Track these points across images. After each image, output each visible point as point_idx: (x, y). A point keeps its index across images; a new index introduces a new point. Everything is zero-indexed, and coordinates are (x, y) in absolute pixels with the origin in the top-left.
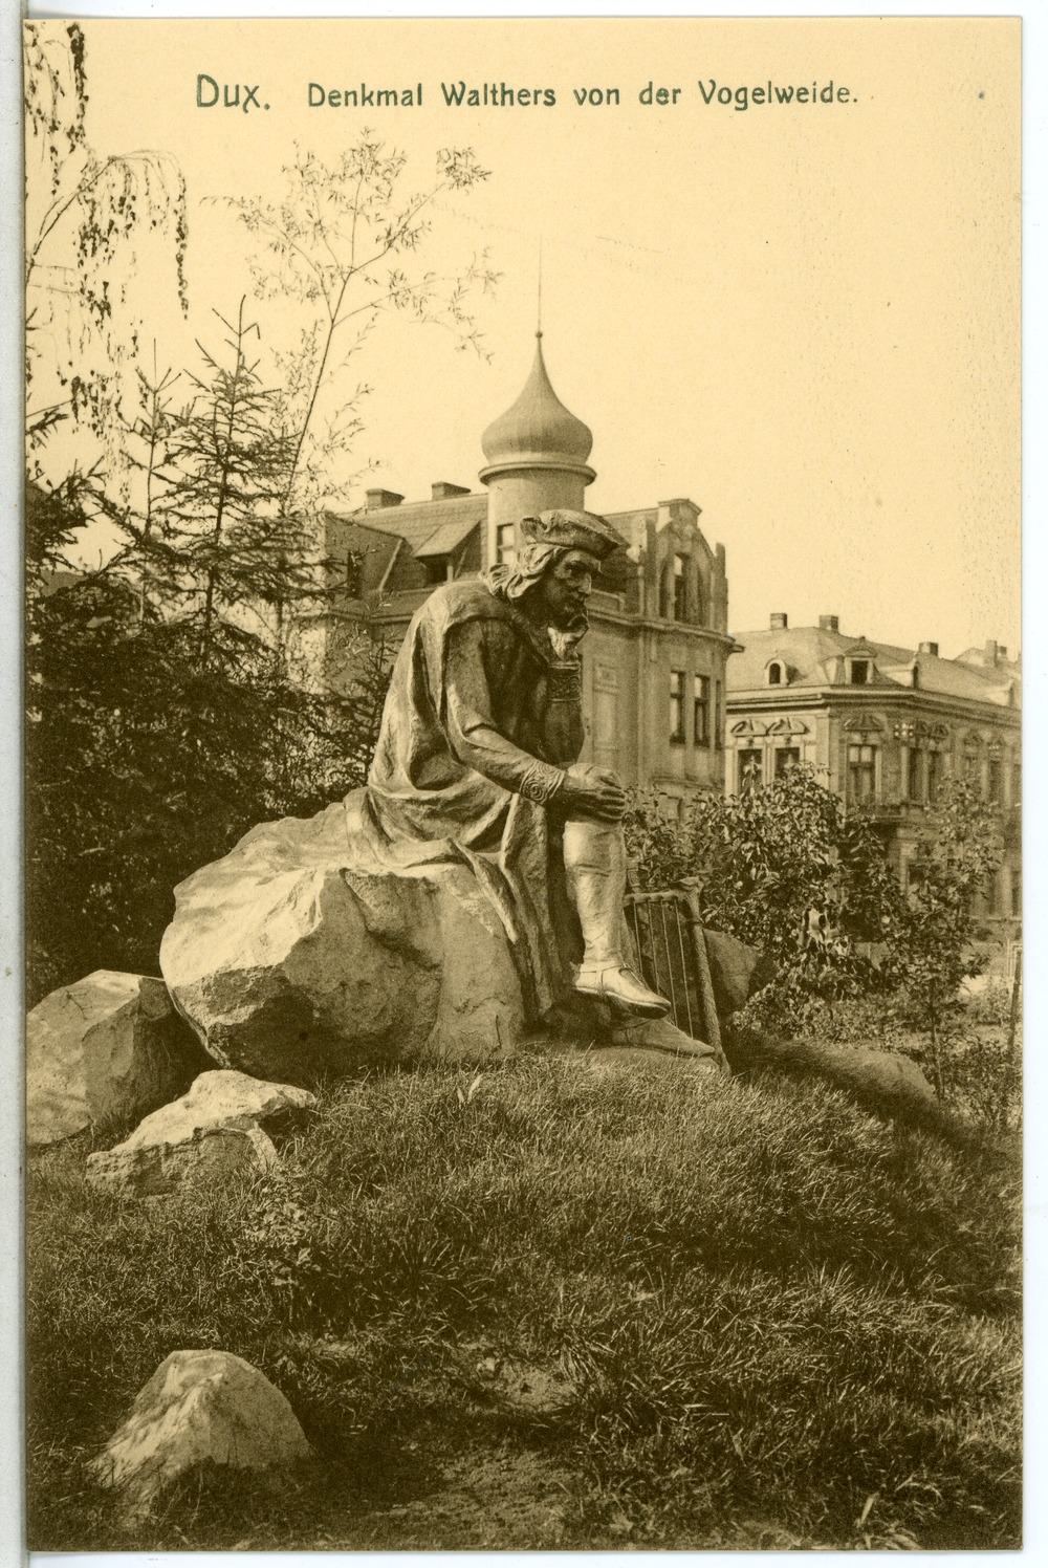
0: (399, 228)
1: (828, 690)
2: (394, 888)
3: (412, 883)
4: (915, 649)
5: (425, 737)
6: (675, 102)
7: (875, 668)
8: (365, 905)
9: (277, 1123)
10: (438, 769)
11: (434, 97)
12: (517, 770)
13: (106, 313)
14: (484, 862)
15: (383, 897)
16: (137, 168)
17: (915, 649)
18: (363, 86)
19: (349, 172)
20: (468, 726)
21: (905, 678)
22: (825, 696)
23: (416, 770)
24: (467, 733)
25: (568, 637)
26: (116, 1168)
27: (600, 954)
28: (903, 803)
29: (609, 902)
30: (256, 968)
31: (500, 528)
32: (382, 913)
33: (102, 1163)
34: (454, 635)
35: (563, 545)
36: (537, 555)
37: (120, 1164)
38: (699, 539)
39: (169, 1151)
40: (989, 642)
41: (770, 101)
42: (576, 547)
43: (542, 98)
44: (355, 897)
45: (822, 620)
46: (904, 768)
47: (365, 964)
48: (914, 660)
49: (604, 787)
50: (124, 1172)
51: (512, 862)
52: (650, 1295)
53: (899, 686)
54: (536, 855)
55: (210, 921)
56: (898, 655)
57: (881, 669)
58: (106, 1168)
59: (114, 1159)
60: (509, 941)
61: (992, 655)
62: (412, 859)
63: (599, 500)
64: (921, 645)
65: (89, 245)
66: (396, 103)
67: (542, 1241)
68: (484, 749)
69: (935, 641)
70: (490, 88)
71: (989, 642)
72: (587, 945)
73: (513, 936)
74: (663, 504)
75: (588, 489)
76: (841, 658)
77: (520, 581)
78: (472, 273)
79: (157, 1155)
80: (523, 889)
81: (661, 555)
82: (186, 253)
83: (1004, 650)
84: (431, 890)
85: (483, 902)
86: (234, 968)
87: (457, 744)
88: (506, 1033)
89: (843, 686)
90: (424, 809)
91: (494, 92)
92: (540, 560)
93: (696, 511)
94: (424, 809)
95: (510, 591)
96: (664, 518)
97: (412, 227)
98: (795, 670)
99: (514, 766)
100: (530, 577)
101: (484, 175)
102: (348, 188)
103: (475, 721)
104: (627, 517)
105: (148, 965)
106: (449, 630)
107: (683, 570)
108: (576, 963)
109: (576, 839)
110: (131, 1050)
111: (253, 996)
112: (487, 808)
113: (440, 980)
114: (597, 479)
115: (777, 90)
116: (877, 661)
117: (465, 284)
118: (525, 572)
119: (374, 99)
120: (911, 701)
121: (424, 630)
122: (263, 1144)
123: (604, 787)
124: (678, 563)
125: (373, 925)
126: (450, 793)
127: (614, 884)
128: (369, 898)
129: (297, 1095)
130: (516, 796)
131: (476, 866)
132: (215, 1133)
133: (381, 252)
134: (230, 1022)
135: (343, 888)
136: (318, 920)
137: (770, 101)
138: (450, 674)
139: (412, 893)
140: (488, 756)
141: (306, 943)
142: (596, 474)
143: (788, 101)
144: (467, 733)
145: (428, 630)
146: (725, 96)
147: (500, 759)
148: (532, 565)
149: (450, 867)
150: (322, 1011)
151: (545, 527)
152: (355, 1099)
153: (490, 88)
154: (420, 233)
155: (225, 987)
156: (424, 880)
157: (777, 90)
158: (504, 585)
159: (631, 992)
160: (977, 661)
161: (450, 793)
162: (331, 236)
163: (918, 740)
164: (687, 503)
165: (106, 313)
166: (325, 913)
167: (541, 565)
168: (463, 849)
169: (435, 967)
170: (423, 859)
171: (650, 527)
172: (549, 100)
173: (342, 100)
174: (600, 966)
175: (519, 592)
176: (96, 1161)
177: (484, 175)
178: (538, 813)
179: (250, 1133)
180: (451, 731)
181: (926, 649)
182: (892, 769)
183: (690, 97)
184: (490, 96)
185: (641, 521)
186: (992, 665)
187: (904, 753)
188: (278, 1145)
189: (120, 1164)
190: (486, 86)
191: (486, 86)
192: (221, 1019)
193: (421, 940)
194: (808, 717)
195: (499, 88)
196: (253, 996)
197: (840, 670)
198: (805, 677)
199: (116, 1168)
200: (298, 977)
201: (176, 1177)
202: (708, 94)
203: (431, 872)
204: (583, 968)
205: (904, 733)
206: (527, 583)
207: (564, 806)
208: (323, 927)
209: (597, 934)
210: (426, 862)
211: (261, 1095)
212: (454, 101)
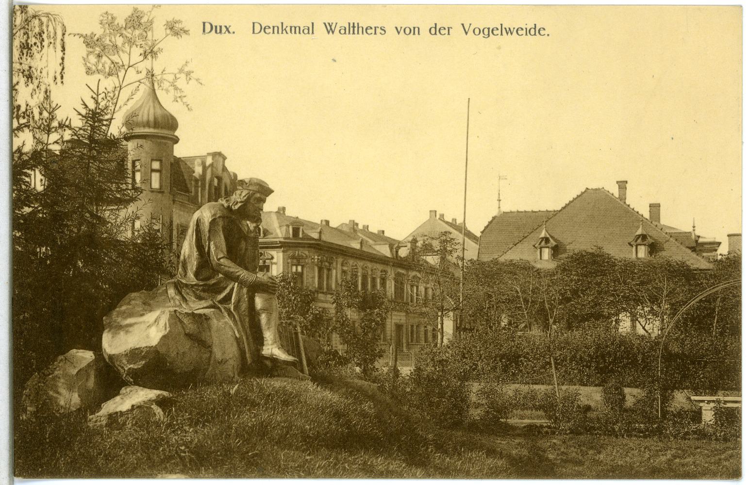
0: (150, 51)
1: (282, 240)
2: (194, 318)
3: (200, 315)
4: (319, 222)
5: (200, 261)
6: (449, 34)
7: (303, 231)
8: (184, 324)
9: (162, 402)
10: (206, 273)
11: (320, 29)
12: (238, 274)
13: (30, 79)
14: (225, 308)
15: (190, 321)
16: (44, 20)
17: (319, 222)
18: (282, 23)
19: (129, 26)
20: (219, 257)
21: (315, 236)
22: (280, 242)
23: (197, 275)
24: (219, 260)
25: (254, 225)
26: (100, 421)
27: (270, 342)
28: (316, 291)
29: (273, 323)
30: (146, 347)
31: (134, 162)
32: (191, 327)
33: (94, 420)
34: (213, 223)
35: (254, 191)
36: (243, 194)
37: (102, 420)
38: (224, 169)
39: (122, 413)
40: (350, 221)
41: (502, 34)
42: (258, 192)
43: (378, 30)
44: (180, 321)
45: (279, 209)
46: (316, 274)
47: (186, 345)
48: (320, 228)
49: (271, 281)
50: (104, 423)
51: (237, 307)
52: (311, 457)
53: (313, 239)
54: (244, 306)
55: (131, 329)
56: (312, 225)
57: (305, 231)
58: (96, 421)
59: (99, 418)
60: (236, 337)
61: (352, 227)
62: (198, 307)
63: (179, 151)
64: (322, 221)
65: (25, 51)
66: (300, 33)
67: (271, 440)
68: (225, 266)
69: (327, 219)
70: (351, 25)
71: (350, 221)
72: (265, 339)
73: (238, 335)
74: (209, 154)
75: (176, 146)
76: (288, 226)
77: (237, 204)
78: (181, 71)
79: (117, 415)
80: (240, 318)
81: (208, 177)
82: (65, 57)
83: (357, 224)
84: (207, 318)
85: (226, 323)
86: (138, 347)
87: (214, 263)
88: (236, 373)
89: (289, 238)
90: (200, 288)
91: (354, 27)
92: (245, 196)
93: (224, 158)
94: (200, 288)
95: (233, 207)
96: (209, 161)
97: (155, 49)
98: (267, 231)
99: (237, 272)
100: (241, 202)
101: (186, 32)
102: (128, 33)
103: (222, 255)
104: (193, 158)
105: (97, 347)
106: (212, 221)
107: (218, 184)
108: (260, 346)
109: (259, 302)
110: (93, 379)
111: (144, 358)
112: (225, 288)
113: (211, 352)
114: (180, 141)
115: (505, 28)
116: (304, 228)
117: (178, 76)
118: (239, 200)
119: (288, 29)
120: (318, 246)
121: (200, 220)
122: (158, 410)
123: (271, 281)
124: (216, 180)
125: (187, 331)
126: (213, 281)
127: (275, 315)
128: (185, 321)
129: (165, 393)
130: (236, 284)
131: (223, 310)
132: (139, 407)
133: (142, 59)
134: (136, 367)
135: (175, 318)
136: (168, 330)
137: (502, 34)
138: (212, 238)
139: (200, 319)
140: (227, 269)
141: (164, 337)
142: (179, 139)
143: (333, 32)
144: (219, 260)
145: (201, 220)
146: (477, 31)
147: (231, 270)
148: (242, 197)
149: (213, 310)
150: (170, 363)
151: (247, 184)
152: (190, 395)
153: (351, 25)
154: (158, 53)
155: (134, 354)
156: (204, 314)
157: (505, 28)
158: (231, 205)
159: (282, 355)
160: (345, 229)
161: (213, 281)
162: (121, 53)
163: (322, 263)
164: (220, 154)
165: (30, 79)
166: (170, 326)
167: (245, 198)
168: (216, 303)
169: (210, 347)
170: (202, 307)
171: (203, 164)
172: (383, 32)
173: (271, 30)
174: (270, 347)
175: (237, 207)
176: (92, 419)
177: (186, 32)
178: (245, 290)
179: (152, 406)
180: (211, 258)
181: (324, 223)
182: (311, 275)
183: (457, 31)
184: (352, 29)
185: (199, 161)
186: (352, 231)
187: (316, 269)
188: (163, 410)
189: (102, 420)
190: (349, 24)
191: (349, 24)
192: (132, 366)
193: (204, 336)
194: (274, 253)
195: (356, 25)
196: (144, 358)
197: (287, 231)
198: (272, 234)
199: (100, 421)
200: (163, 350)
201: (124, 424)
202: (399, 30)
203: (207, 311)
204: (264, 348)
205: (316, 260)
206: (239, 205)
207: (255, 288)
208: (170, 331)
209: (269, 335)
210: (203, 308)
211: (151, 394)
212: (509, 33)
